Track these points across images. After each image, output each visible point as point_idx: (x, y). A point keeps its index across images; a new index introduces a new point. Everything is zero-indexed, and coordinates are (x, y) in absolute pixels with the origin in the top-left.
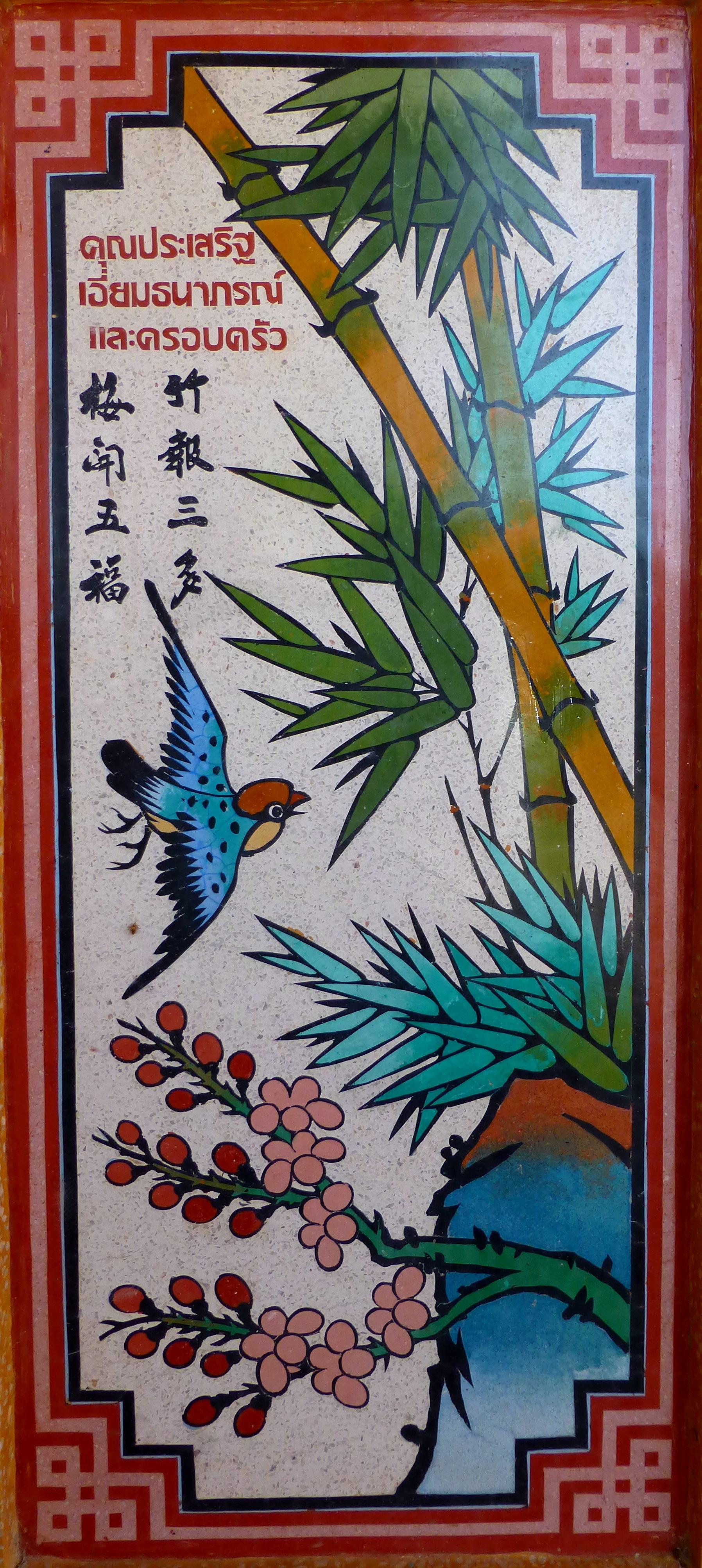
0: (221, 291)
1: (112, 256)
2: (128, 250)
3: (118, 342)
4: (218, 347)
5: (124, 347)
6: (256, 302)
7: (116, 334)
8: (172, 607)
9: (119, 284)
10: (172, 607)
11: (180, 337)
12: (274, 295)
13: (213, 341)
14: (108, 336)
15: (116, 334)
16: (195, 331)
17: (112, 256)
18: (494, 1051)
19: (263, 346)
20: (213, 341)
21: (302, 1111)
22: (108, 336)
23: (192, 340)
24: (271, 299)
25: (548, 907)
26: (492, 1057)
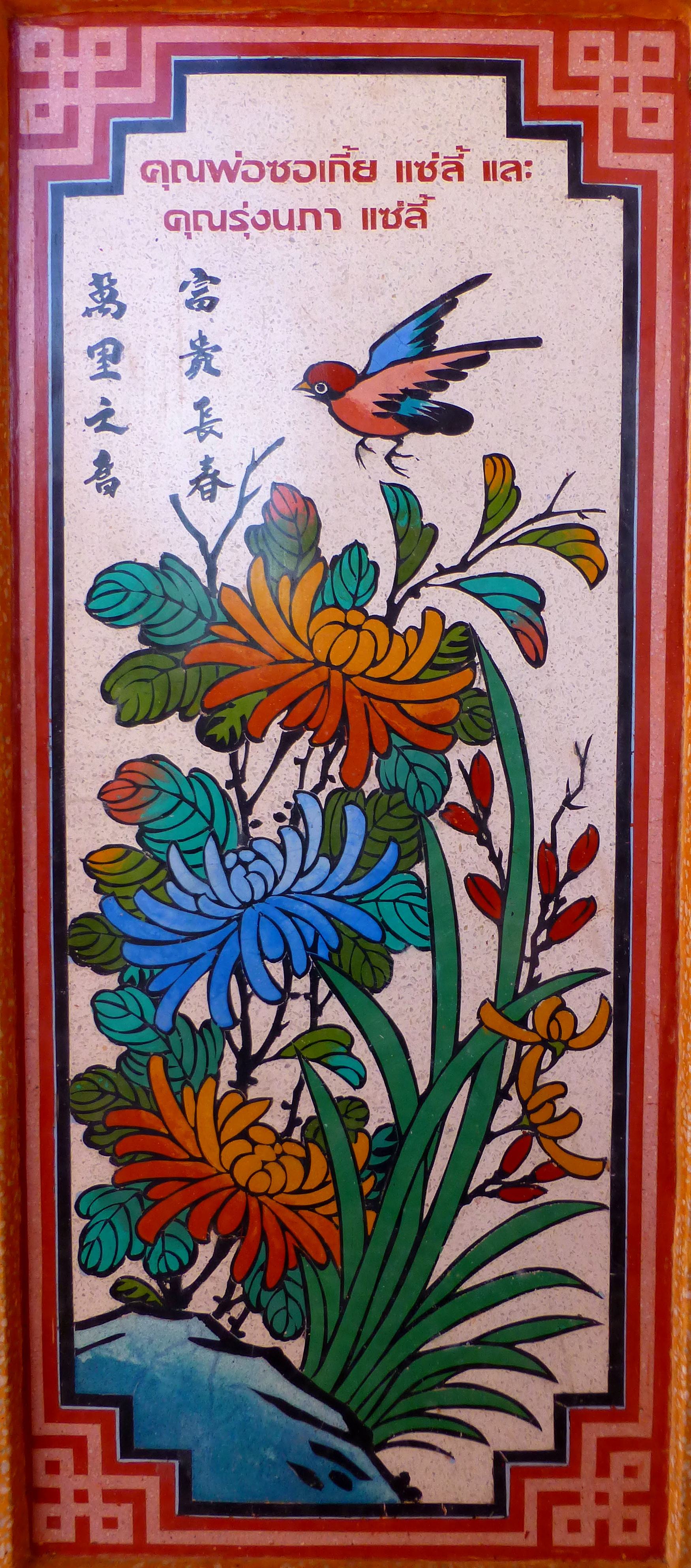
1: (176, 180)
3: (513, 175)
5: (519, 178)
7: (512, 166)
9: (363, 162)
12: (196, 174)
15: (512, 166)
17: (176, 180)
22: (500, 170)
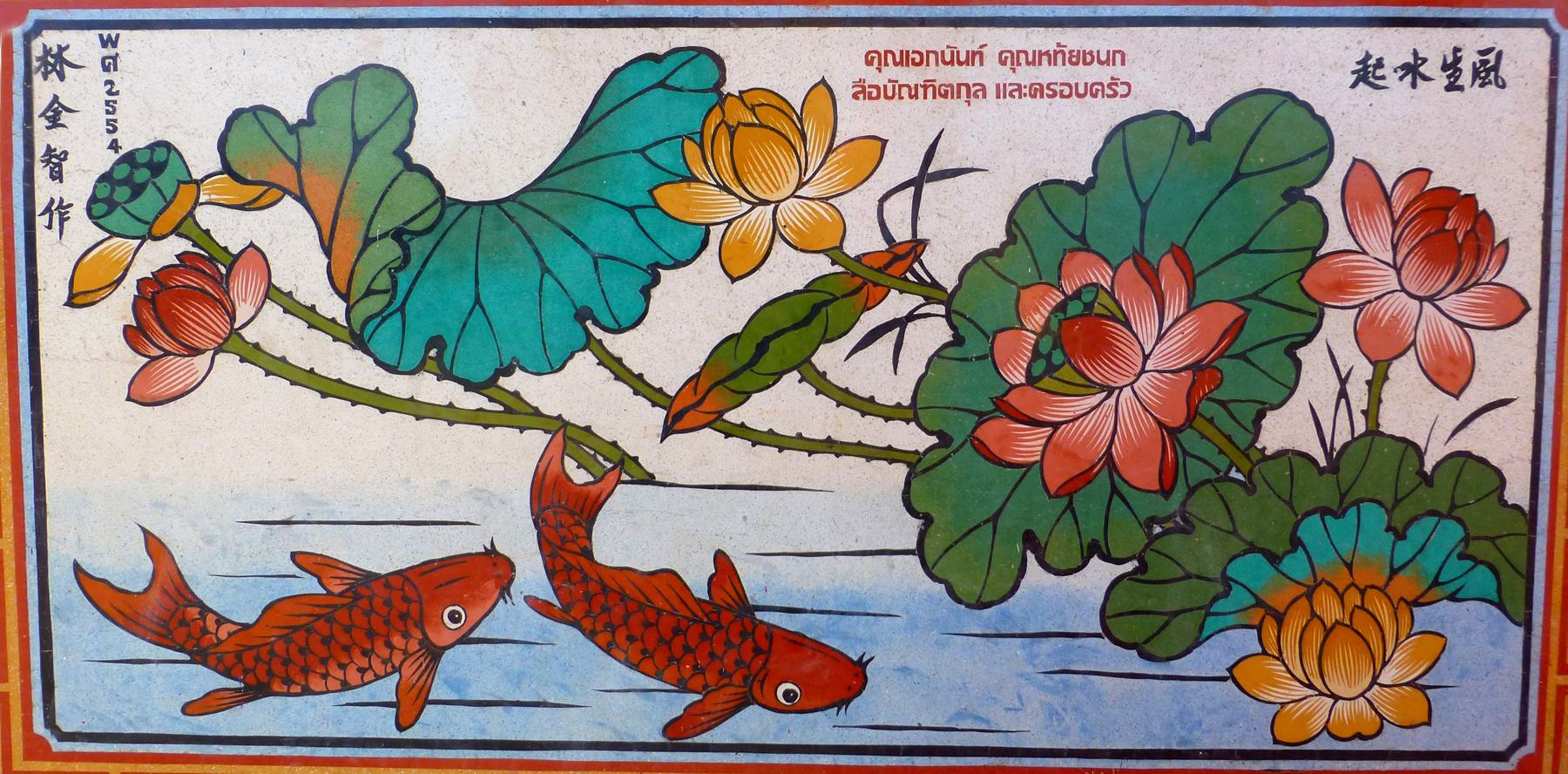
0: (963, 89)
2: (890, 56)
4: (1084, 96)
6: (901, 98)
8: (74, 300)
10: (74, 300)
11: (1058, 88)
13: (1081, 91)
14: (1009, 89)
16: (1069, 85)
18: (375, 239)
19: (1115, 94)
20: (1081, 91)
21: (235, 167)
22: (1009, 89)
23: (1067, 91)
24: (911, 97)
25: (1215, 265)
26: (1253, 601)
